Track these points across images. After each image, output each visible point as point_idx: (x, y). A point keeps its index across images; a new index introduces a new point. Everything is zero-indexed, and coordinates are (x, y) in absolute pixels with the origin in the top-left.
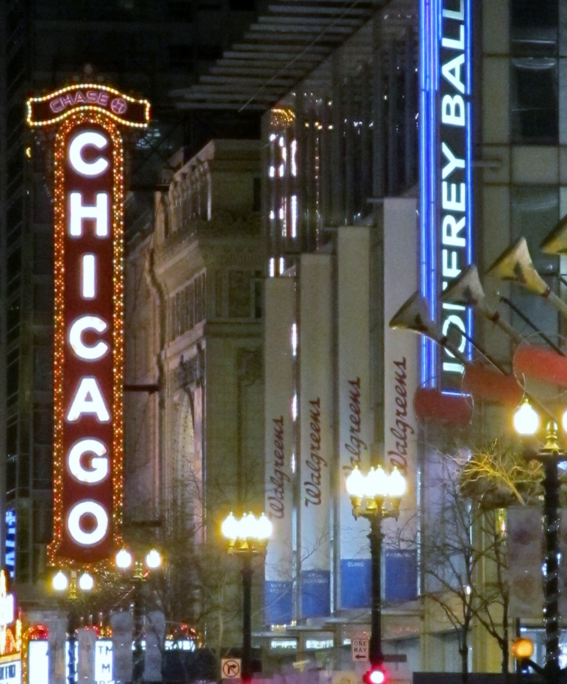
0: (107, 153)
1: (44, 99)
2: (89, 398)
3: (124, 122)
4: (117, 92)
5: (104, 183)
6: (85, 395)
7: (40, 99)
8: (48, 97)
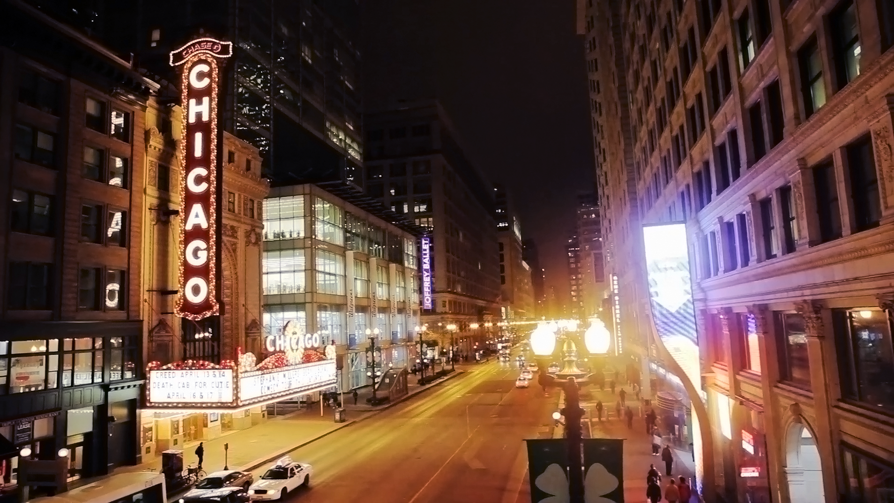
0: (209, 75)
1: (179, 50)
2: (197, 216)
3: (221, 56)
4: (218, 41)
5: (207, 91)
6: (195, 214)
7: (177, 51)
8: (181, 49)
